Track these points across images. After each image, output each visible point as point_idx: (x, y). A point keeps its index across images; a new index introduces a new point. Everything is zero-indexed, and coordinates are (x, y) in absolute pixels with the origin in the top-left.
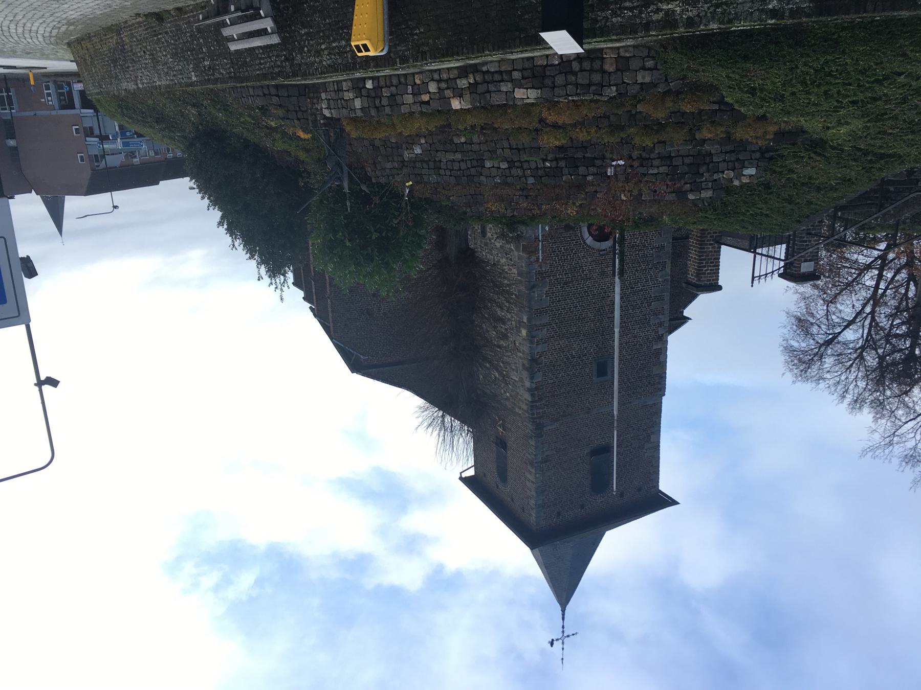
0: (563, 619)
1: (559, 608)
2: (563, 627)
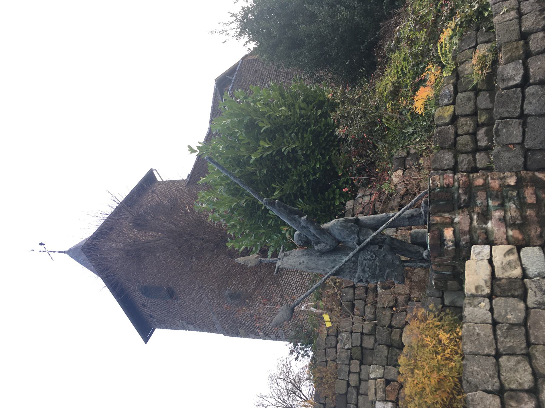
0: (60, 252)
1: (67, 249)
2: (54, 252)
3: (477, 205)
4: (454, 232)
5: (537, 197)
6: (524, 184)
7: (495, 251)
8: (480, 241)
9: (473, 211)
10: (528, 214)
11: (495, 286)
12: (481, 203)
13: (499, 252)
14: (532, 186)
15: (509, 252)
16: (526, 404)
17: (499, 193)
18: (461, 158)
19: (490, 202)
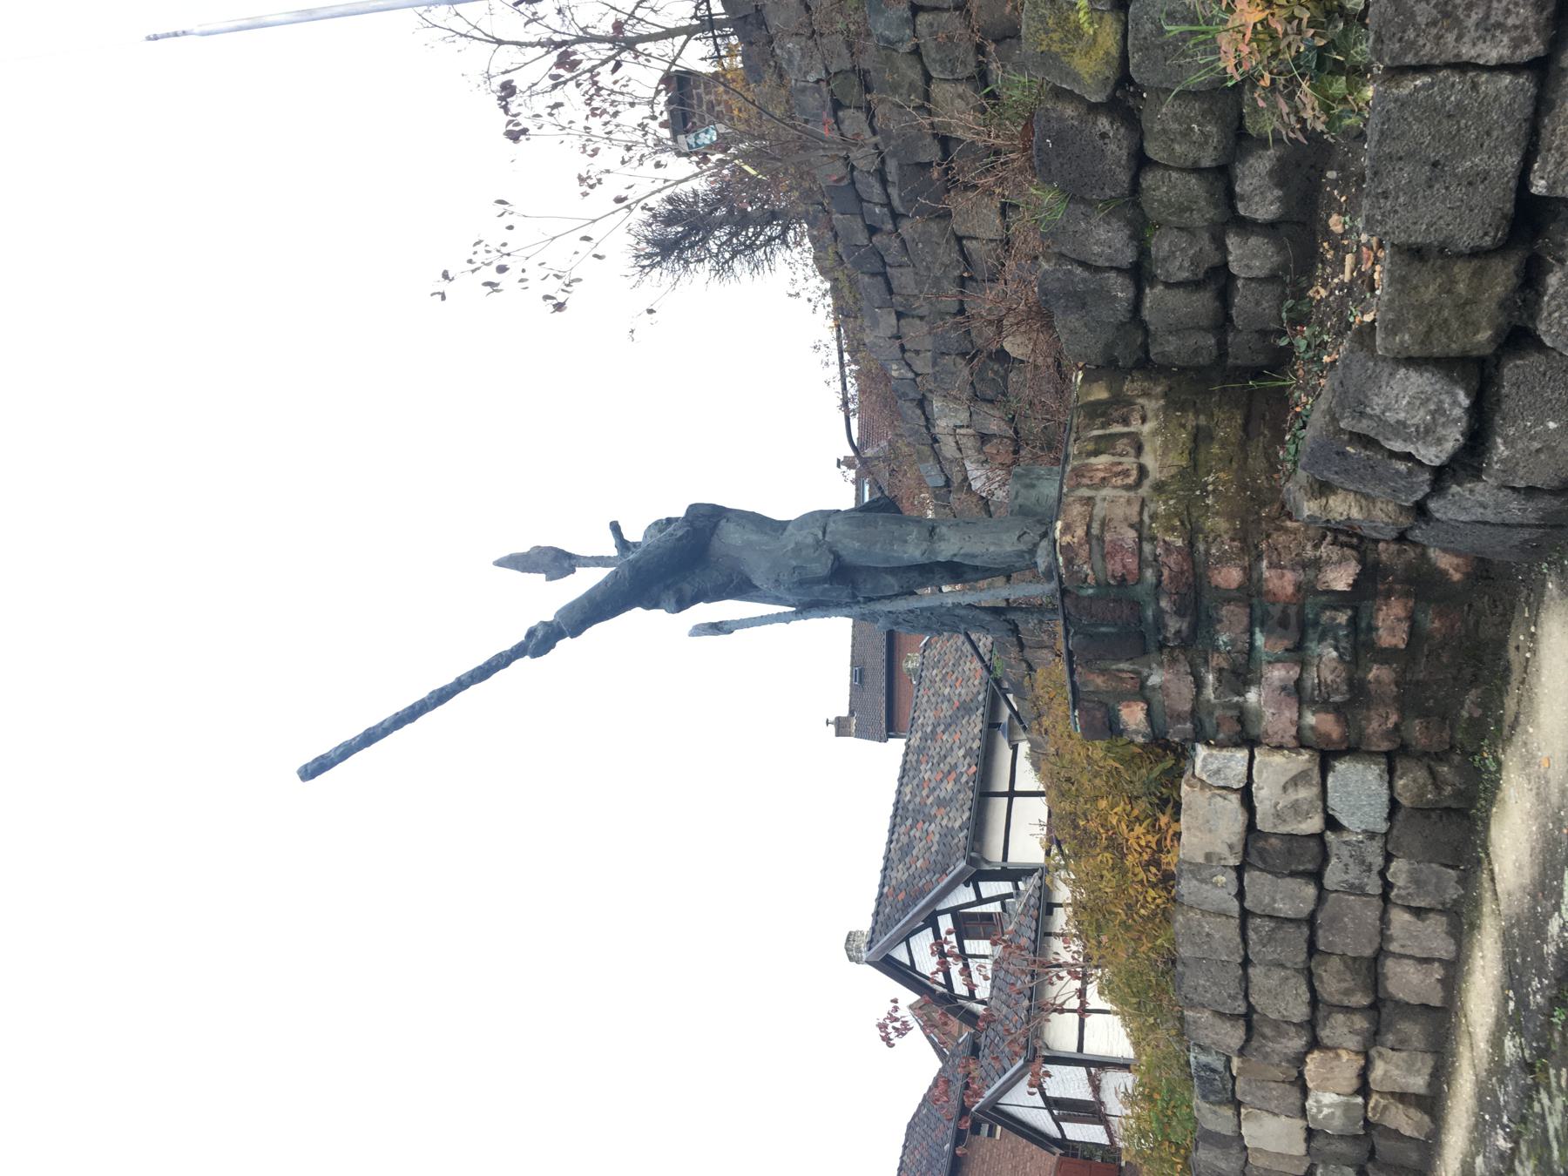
3: (1217, 649)
4: (1149, 714)
5: (1414, 632)
6: (1380, 587)
7: (1260, 772)
8: (1221, 736)
9: (1206, 662)
10: (1371, 676)
11: (1253, 852)
12: (1233, 642)
13: (1275, 773)
14: (1407, 595)
15: (1295, 781)
16: (1291, 1039)
17: (1293, 611)
18: (1166, 246)
19: (1260, 639)
